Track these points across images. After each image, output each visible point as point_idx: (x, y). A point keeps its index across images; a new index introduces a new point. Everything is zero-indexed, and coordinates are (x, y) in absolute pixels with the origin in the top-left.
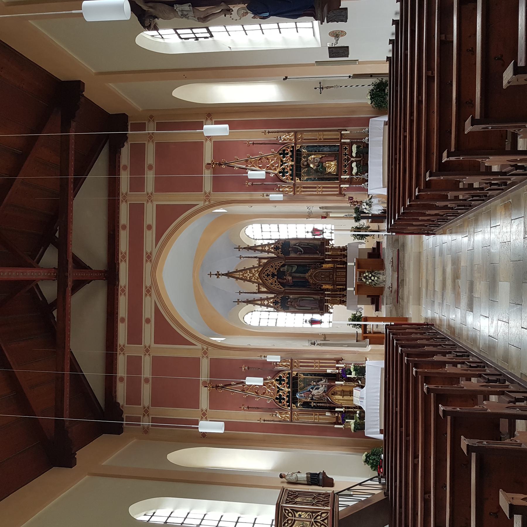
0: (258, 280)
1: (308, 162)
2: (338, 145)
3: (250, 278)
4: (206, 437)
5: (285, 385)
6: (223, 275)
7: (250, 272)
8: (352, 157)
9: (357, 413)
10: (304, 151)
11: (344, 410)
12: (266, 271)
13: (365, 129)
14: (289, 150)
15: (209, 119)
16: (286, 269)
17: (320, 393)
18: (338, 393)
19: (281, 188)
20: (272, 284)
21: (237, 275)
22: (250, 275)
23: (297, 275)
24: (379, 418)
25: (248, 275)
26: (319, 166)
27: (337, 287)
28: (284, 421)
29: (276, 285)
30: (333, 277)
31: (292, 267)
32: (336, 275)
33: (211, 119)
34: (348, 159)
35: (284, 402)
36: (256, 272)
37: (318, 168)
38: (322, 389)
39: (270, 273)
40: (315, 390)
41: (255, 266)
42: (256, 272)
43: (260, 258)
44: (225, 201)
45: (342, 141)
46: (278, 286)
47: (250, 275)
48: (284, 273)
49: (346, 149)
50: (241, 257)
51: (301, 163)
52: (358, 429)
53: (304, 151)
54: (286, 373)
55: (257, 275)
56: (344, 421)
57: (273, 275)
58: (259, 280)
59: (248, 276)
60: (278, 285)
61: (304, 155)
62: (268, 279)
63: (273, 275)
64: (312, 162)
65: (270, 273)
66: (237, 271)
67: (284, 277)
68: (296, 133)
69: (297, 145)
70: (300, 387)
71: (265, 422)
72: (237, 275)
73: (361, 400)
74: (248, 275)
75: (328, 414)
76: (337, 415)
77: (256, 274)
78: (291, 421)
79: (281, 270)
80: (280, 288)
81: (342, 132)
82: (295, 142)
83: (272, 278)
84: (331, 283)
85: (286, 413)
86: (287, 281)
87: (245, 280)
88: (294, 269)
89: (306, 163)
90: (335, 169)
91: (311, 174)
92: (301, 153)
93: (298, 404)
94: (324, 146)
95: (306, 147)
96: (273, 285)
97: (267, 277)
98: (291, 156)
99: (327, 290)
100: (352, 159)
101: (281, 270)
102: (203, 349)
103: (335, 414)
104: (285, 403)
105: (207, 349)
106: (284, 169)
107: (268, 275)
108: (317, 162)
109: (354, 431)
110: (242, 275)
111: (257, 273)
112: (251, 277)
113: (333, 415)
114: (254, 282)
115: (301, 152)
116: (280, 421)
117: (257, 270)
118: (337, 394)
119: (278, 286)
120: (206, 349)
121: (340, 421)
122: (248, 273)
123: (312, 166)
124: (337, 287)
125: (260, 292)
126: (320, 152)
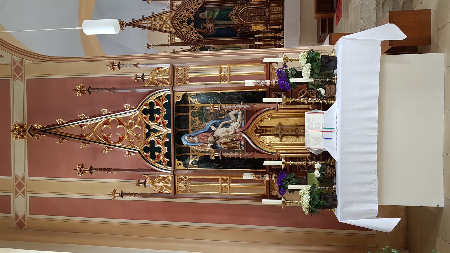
0: (170, 29)
3: (160, 26)
4: (24, 228)
5: (160, 120)
6: (127, 24)
7: (160, 19)
9: (314, 170)
11: (283, 163)
12: (180, 16)
17: (231, 133)
18: (270, 131)
20: (187, 32)
22: (160, 23)
24: (376, 177)
25: (158, 23)
27: (272, 27)
28: (161, 195)
29: (193, 33)
31: (214, 11)
32: (270, 11)
35: (159, 157)
38: (235, 125)
40: (222, 127)
46: (196, 35)
48: (204, 20)
52: (318, 206)
54: (161, 96)
55: (169, 22)
56: (283, 189)
58: (172, 29)
59: (158, 25)
60: (196, 9)
62: (182, 26)
63: (189, 21)
65: (186, 19)
66: (144, 19)
67: (204, 25)
70: (193, 126)
71: (125, 198)
72: (144, 23)
73: (327, 135)
75: (248, 176)
76: (267, 178)
78: (175, 194)
80: (199, 37)
83: (188, 25)
84: (262, 23)
85: (164, 178)
88: (216, 14)
93: (190, 162)
95: (196, 95)
96: (189, 33)
97: (182, 24)
98: (167, 117)
99: (258, 32)
102: (14, 63)
103: (263, 177)
104: (161, 158)
105: (21, 63)
109: (311, 211)
112: (162, 26)
113: (258, 177)
116: (152, 195)
117: (169, 16)
118: (268, 133)
119: (196, 35)
120: (20, 63)
121: (274, 193)
122: (158, 21)
124: (272, 27)
125: (173, 44)
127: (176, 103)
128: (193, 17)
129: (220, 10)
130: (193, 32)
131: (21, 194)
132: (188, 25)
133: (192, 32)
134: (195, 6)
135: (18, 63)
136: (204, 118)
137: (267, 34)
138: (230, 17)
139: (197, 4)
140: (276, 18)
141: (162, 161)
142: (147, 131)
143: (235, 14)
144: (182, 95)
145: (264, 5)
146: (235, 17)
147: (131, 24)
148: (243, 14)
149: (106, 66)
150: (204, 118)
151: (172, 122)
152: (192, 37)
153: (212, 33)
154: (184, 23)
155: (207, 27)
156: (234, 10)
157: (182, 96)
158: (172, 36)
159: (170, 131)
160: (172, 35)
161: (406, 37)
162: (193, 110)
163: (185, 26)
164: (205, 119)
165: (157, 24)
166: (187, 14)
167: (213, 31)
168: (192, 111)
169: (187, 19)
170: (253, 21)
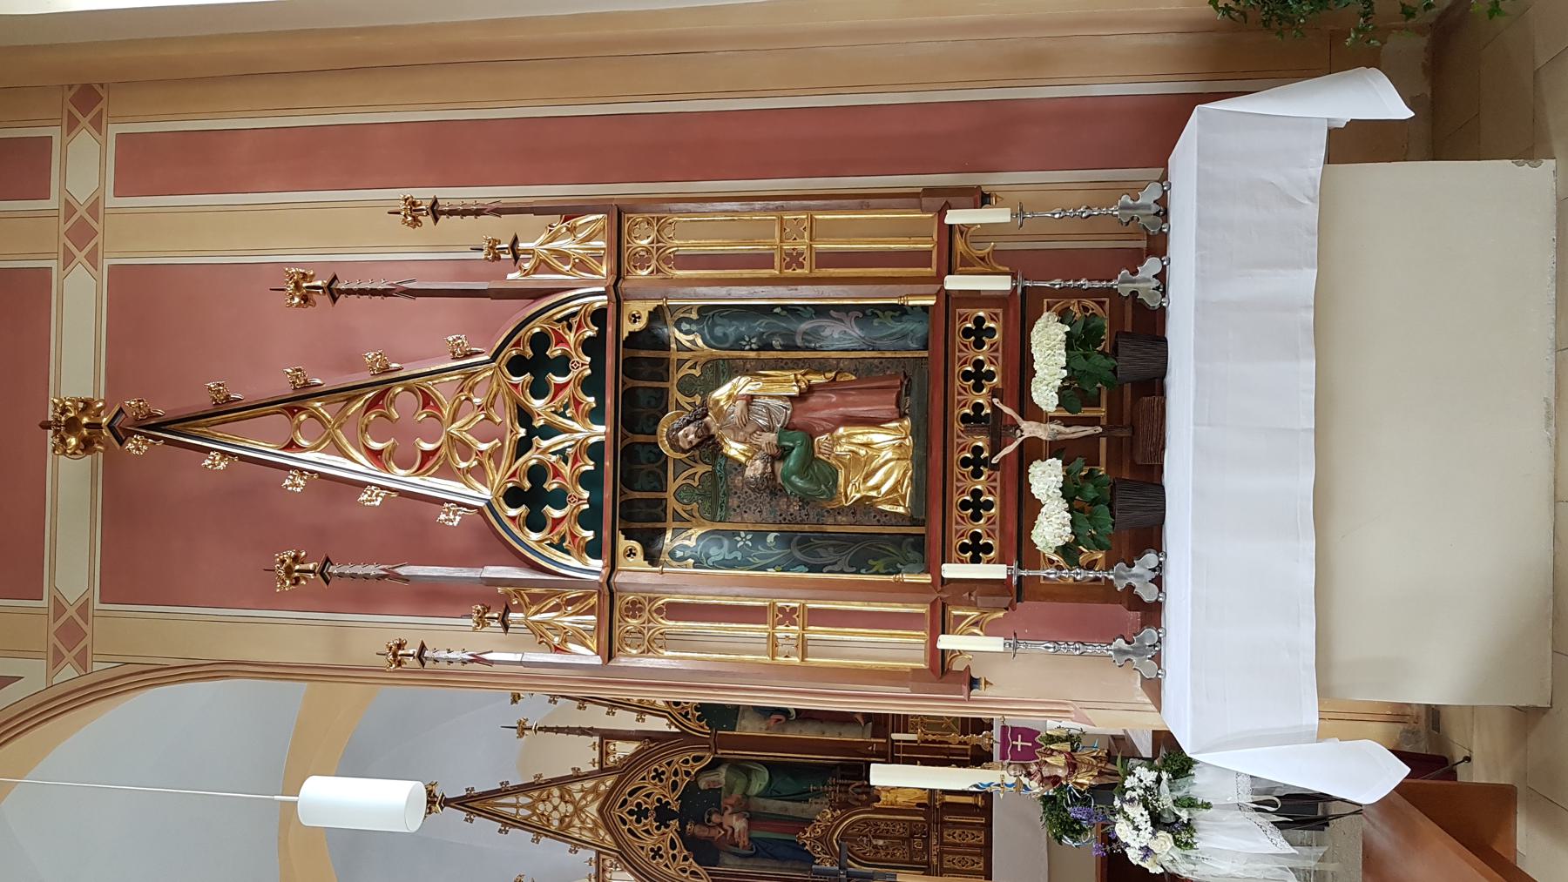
0: (597, 835)
1: (707, 428)
2: (925, 308)
3: (561, 821)
5: (564, 527)
6: (447, 802)
7: (562, 797)
8: (1030, 410)
10: (682, 338)
12: (631, 794)
13: (1135, 189)
14: (571, 337)
15: (85, 121)
16: (724, 780)
19: (518, 609)
20: (656, 853)
21: (507, 806)
23: (774, 806)
26: (782, 454)
29: (674, 857)
30: (927, 848)
33: (97, 124)
34: (999, 430)
36: (589, 798)
37: (779, 467)
39: (651, 804)
41: (583, 770)
42: (589, 798)
43: (608, 736)
44: (173, 663)
45: (953, 283)
47: (562, 808)
48: (714, 799)
49: (979, 334)
50: (522, 729)
51: (663, 429)
53: (682, 338)
54: (574, 314)
55: (593, 810)
57: (663, 814)
59: (556, 815)
60: (686, 859)
61: (685, 370)
63: (663, 814)
64: (735, 429)
65: (651, 804)
66: (504, 791)
68: (619, 214)
69: (632, 307)
72: (507, 806)
74: (554, 808)
77: (586, 805)
79: (703, 785)
81: (953, 217)
82: (611, 281)
83: (658, 828)
86: (725, 835)
87: (540, 829)
89: (689, 434)
90: (899, 483)
91: (734, 502)
92: (663, 354)
94: (821, 311)
95: (694, 316)
97: (638, 821)
98: (592, 385)
100: (1030, 429)
101: (703, 785)
106: (538, 473)
107: (641, 813)
108: (771, 429)
110: (527, 806)
111: (592, 801)
112: (567, 820)
114: (578, 844)
115: (665, 346)
117: (595, 789)
123: (734, 449)
126: (798, 349)
127: (627, 338)
128: (677, 800)
129: (770, 776)
130: (673, 778)
131: (67, 606)
132: (658, 828)
133: (677, 779)
134: (682, 762)
135: (81, 211)
136: (721, 507)
137: (934, 735)
138: (805, 844)
139: (690, 759)
140: (963, 859)
141: (568, 538)
142: (522, 432)
143: (822, 837)
144: (650, 312)
145: (920, 816)
146: (822, 849)
147: (461, 803)
148: (850, 832)
149: (389, 213)
150: (721, 507)
151: (609, 401)
152: (672, 872)
153: (740, 850)
154: (646, 818)
155: (725, 826)
156: (819, 823)
157: (647, 315)
158: (604, 860)
159: (599, 432)
160: (602, 856)
161: (1413, 114)
162: (684, 482)
163: (648, 829)
164: (724, 508)
165: (550, 802)
166: (658, 791)
167: (746, 844)
168: (680, 481)
169: (657, 807)
170: (883, 858)
